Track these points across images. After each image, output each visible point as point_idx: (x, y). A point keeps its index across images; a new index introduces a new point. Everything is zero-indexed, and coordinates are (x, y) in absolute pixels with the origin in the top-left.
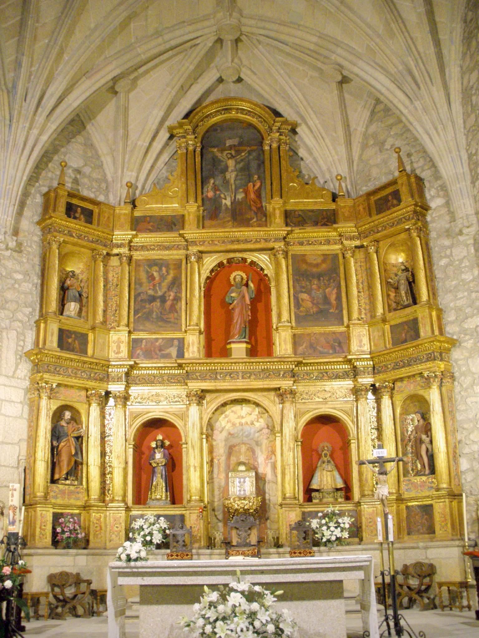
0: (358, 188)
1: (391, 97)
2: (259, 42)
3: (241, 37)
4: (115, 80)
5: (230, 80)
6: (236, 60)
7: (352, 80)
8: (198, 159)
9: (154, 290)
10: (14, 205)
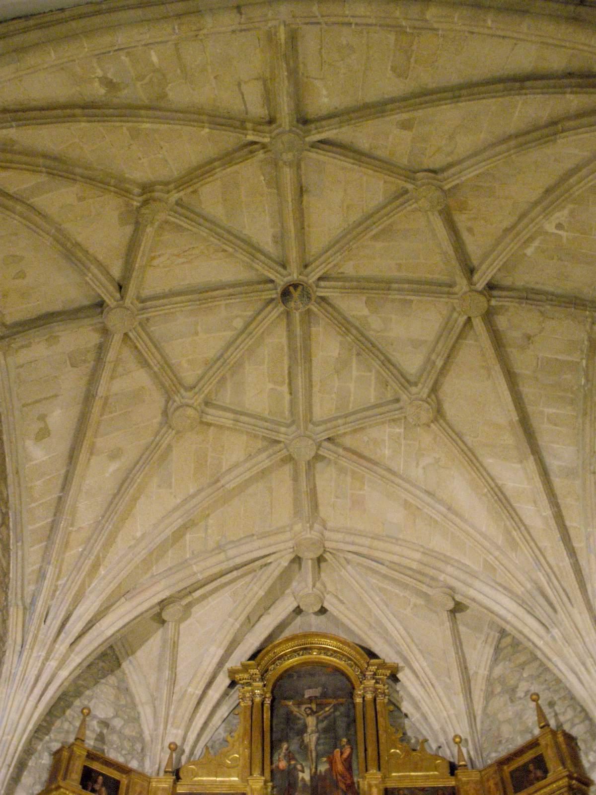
0: (484, 755)
1: (519, 625)
2: (348, 562)
3: (325, 555)
4: (163, 604)
5: (311, 611)
6: (318, 585)
7: (467, 607)
8: (267, 715)
10: (9, 766)
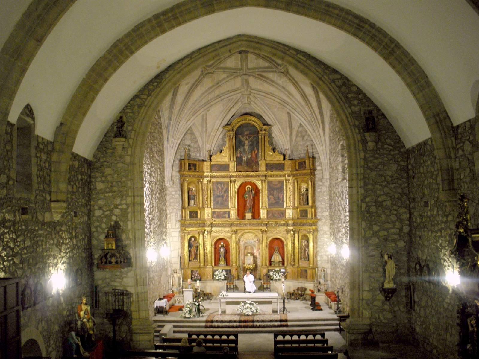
9: (220, 193)
